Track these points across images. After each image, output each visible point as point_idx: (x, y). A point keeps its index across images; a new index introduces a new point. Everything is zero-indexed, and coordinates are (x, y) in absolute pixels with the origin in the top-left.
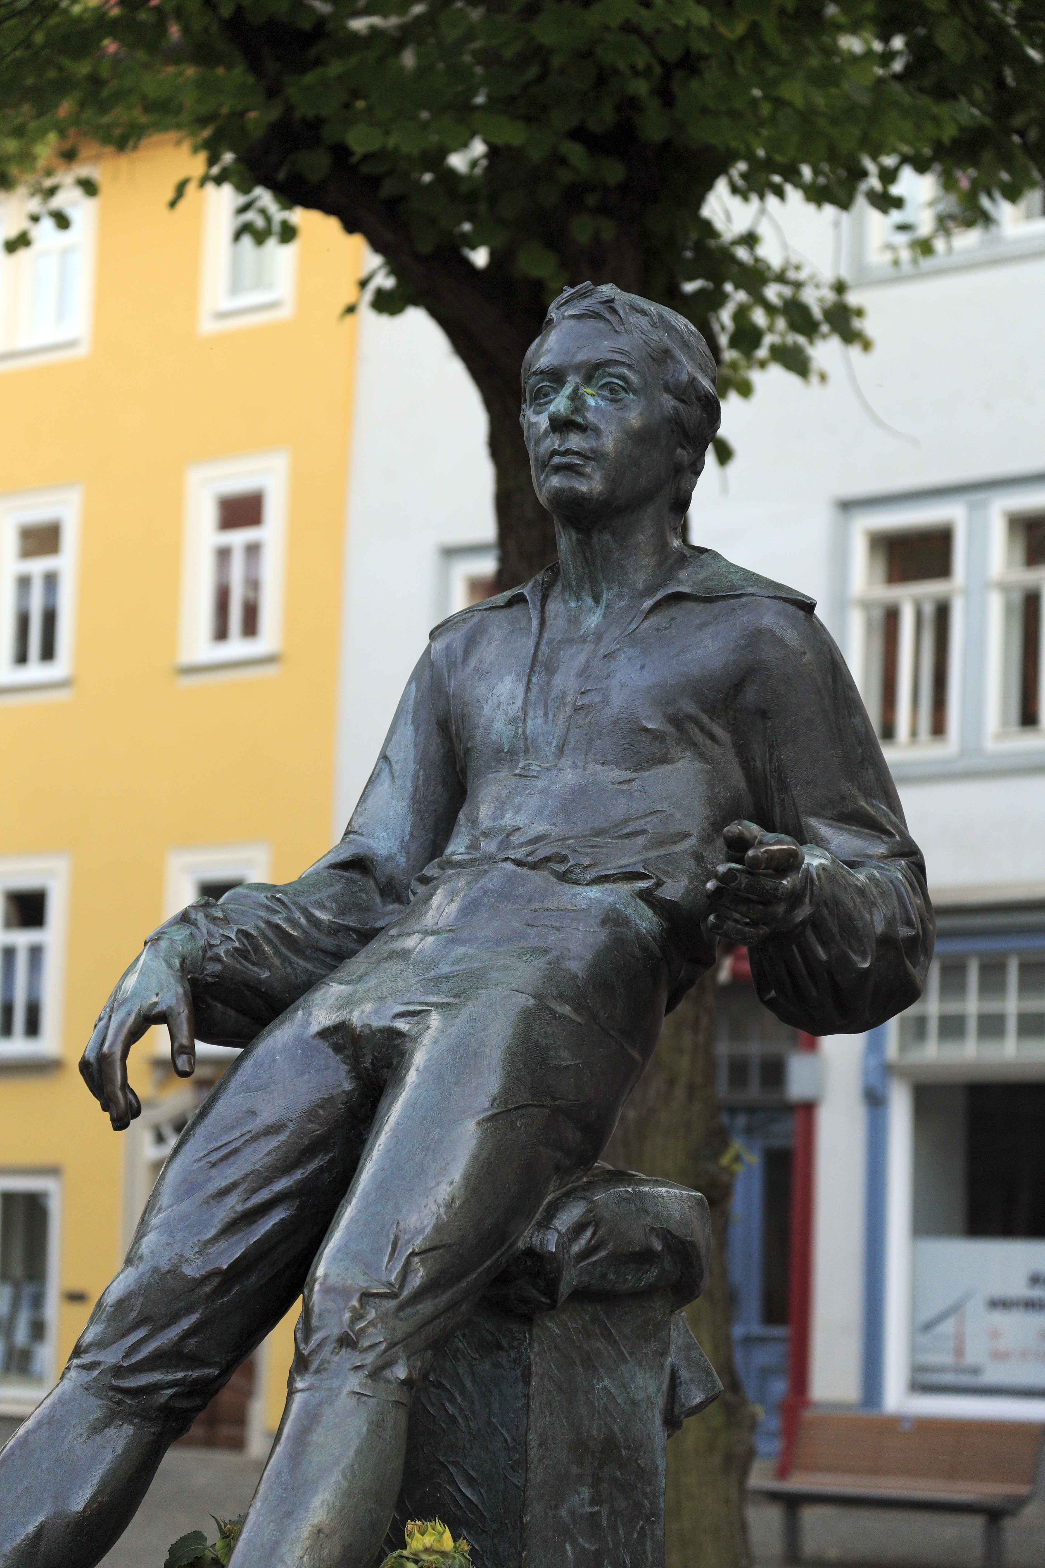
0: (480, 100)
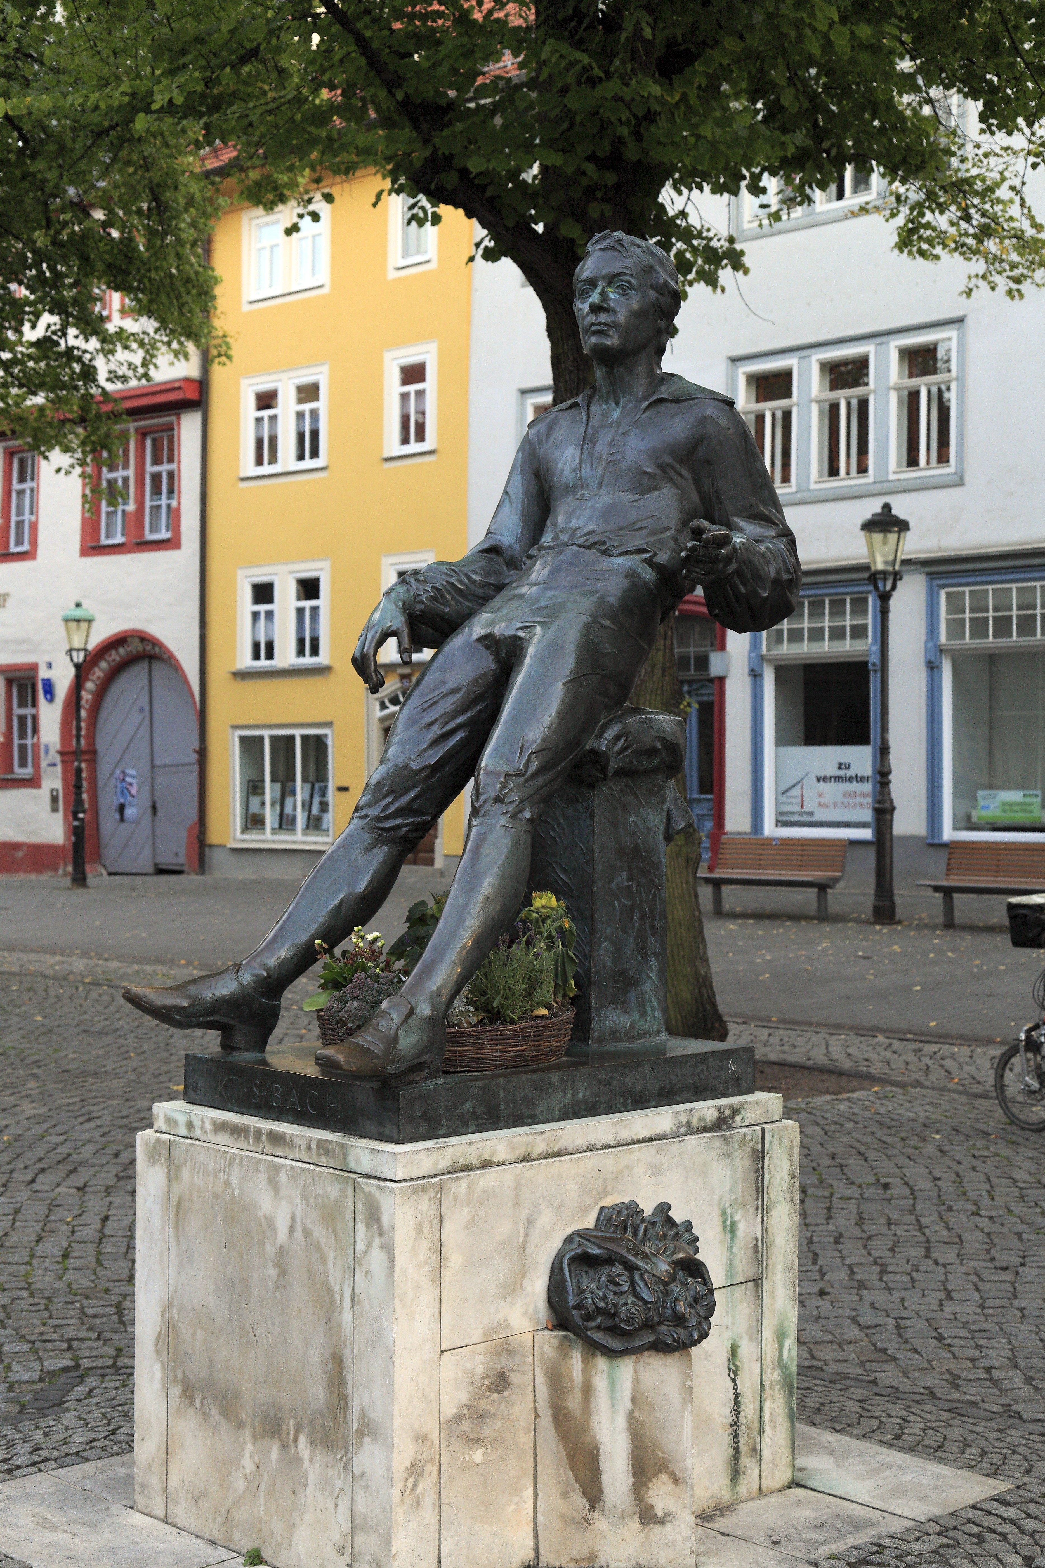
0: (538, 141)
